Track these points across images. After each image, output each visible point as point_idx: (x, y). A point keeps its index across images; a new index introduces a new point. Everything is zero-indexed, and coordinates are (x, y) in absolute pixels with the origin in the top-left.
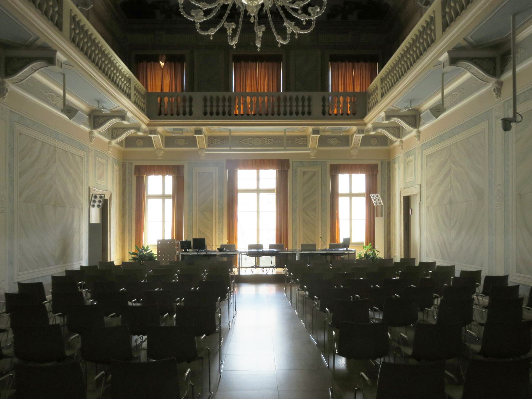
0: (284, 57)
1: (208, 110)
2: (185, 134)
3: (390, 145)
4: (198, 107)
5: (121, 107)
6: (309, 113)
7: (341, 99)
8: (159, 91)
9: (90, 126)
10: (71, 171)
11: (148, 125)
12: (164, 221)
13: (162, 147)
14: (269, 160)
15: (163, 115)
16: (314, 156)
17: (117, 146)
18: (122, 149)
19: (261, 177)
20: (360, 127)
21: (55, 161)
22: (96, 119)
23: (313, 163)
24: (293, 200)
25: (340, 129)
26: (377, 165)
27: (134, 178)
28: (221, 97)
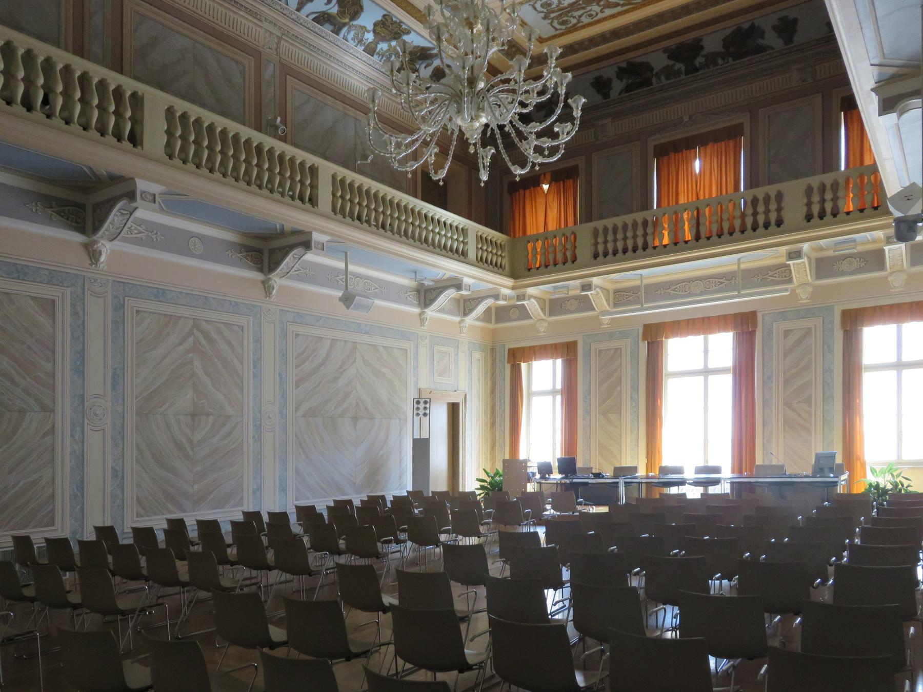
0: (747, 129)
1: (601, 248)
2: (860, 248)
4: (794, 209)
5: (448, 274)
6: (779, 223)
7: (530, 246)
8: (541, 230)
9: (419, 305)
10: (384, 370)
13: (608, 308)
14: (719, 316)
15: (703, 240)
17: (479, 324)
18: (491, 326)
21: (355, 361)
22: (426, 295)
23: (806, 313)
24: (764, 383)
25: (854, 241)
27: (508, 368)
28: (630, 223)
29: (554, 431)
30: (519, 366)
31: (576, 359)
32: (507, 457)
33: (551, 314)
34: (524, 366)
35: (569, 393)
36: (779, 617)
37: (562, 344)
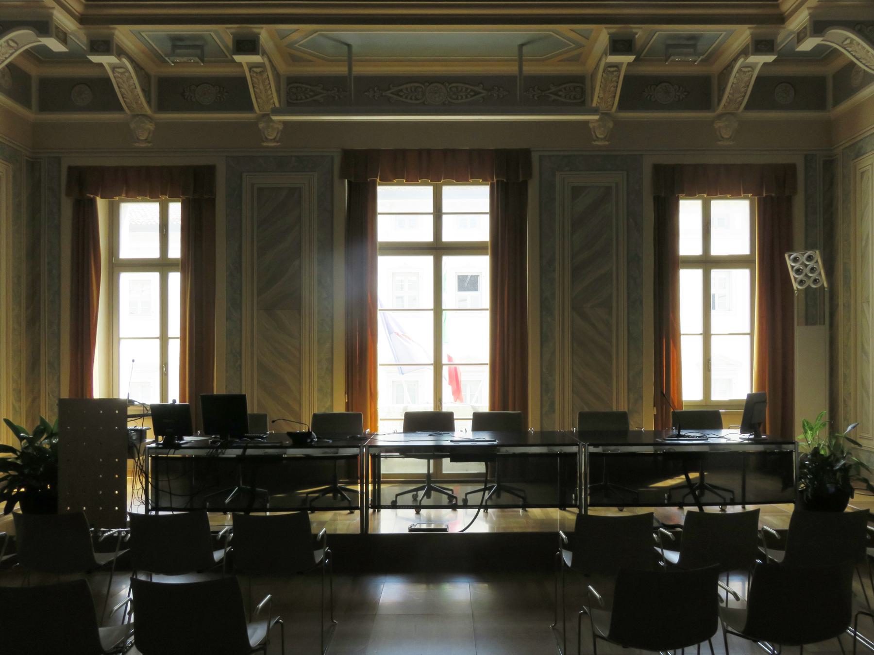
3: (837, 102)
11: (83, 20)
12: (164, 338)
13: (148, 111)
16: (605, 139)
18: (31, 115)
19: (447, 206)
20: (765, 30)
26: (792, 168)
29: (164, 338)
30: (93, 204)
31: (212, 201)
32: (65, 394)
33: (162, 107)
34: (101, 204)
35: (199, 262)
36: (258, 489)
37: (183, 170)
